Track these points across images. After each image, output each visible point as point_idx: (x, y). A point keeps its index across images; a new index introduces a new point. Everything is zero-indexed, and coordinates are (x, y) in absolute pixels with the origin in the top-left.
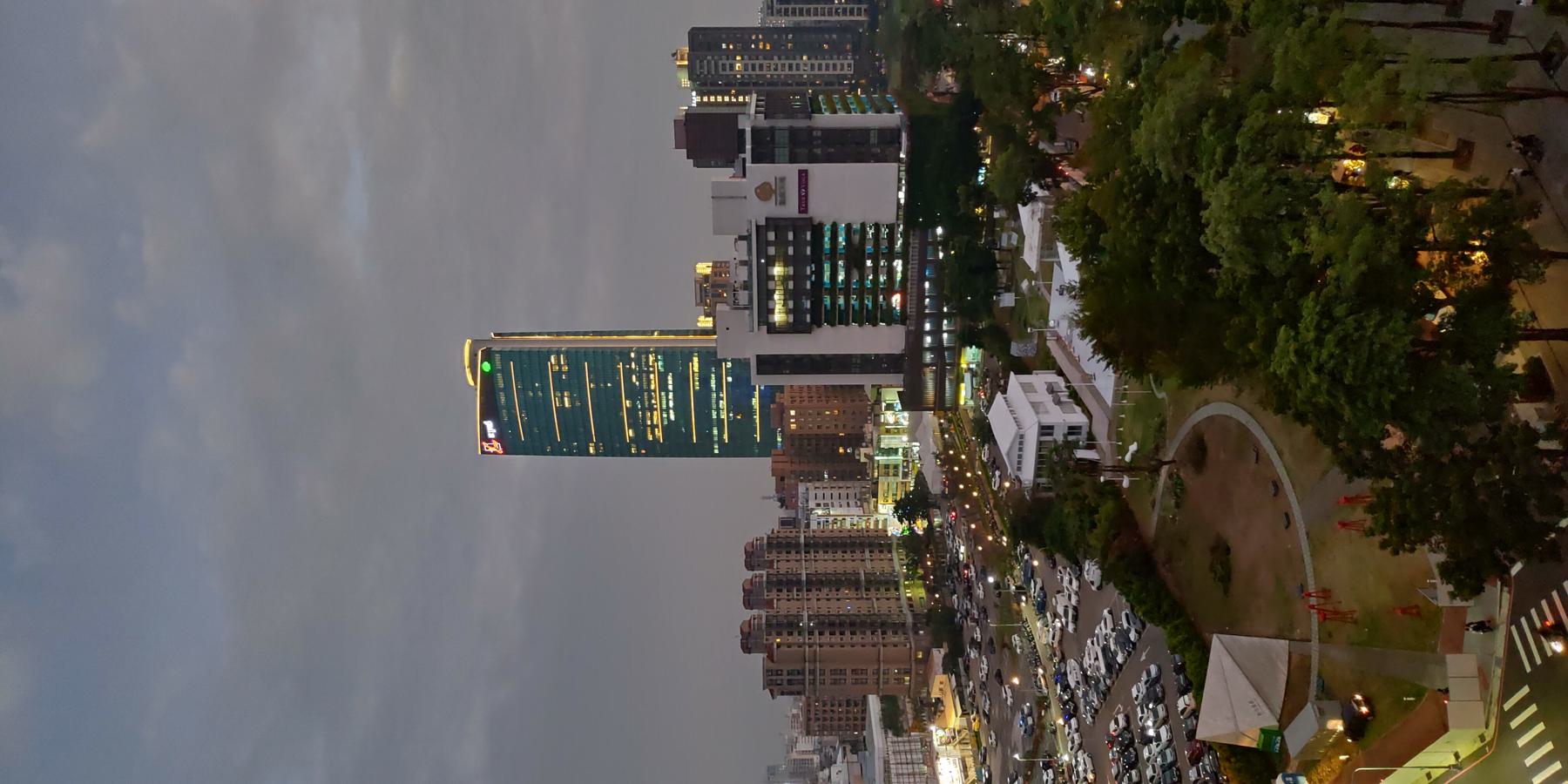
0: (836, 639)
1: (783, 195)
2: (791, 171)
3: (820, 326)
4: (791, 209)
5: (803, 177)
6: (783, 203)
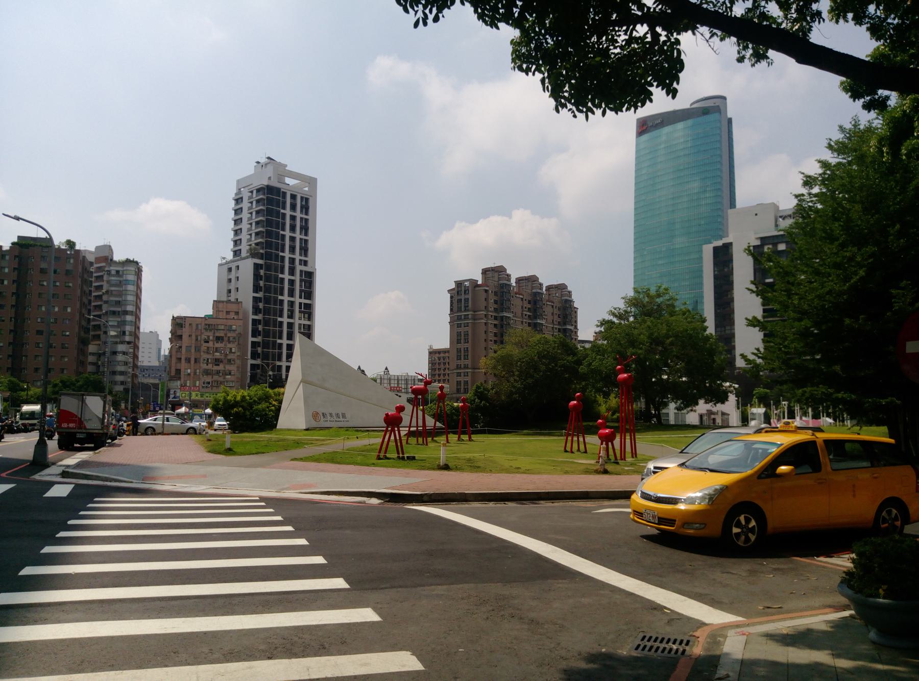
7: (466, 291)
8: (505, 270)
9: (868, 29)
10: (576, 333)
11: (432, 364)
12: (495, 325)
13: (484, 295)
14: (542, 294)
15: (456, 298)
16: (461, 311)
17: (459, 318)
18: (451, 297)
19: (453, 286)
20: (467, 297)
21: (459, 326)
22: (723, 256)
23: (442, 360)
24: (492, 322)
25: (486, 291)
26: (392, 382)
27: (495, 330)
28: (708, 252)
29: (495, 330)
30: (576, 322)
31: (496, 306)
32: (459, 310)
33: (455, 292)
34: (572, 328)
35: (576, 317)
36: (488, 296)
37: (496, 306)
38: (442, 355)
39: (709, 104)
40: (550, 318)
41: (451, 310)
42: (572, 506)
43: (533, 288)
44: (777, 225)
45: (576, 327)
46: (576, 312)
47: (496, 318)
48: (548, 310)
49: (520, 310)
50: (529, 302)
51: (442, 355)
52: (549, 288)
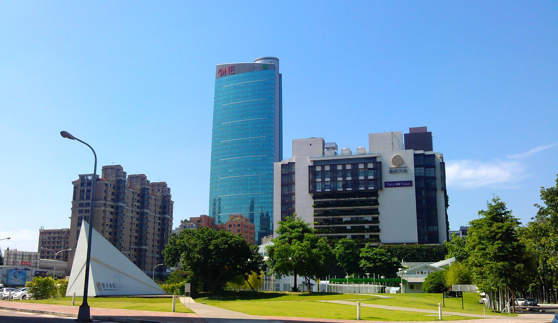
0: (108, 222)
1: (396, 172)
2: (411, 176)
3: (314, 198)
4: (387, 177)
5: (408, 184)
6: (391, 172)
7: (89, 183)
8: (122, 169)
9: (375, 163)
10: (171, 221)
11: (42, 242)
12: (111, 213)
13: (104, 188)
14: (125, 181)
15: (80, 188)
16: (83, 199)
17: (81, 205)
18: (75, 188)
19: (78, 178)
20: (89, 188)
21: (81, 211)
22: (288, 171)
23: (52, 240)
24: (109, 209)
25: (106, 185)
26: (18, 257)
27: (111, 217)
28: (277, 166)
29: (111, 217)
30: (172, 212)
31: (113, 197)
32: (82, 198)
33: (79, 183)
34: (169, 217)
35: (172, 209)
36: (107, 188)
37: (113, 197)
38: (52, 235)
39: (267, 62)
40: (130, 201)
41: (74, 198)
42: (297, 316)
43: (117, 176)
44: (324, 153)
45: (172, 216)
46: (172, 205)
47: (112, 207)
48: (152, 202)
49: (132, 201)
50: (139, 196)
51: (52, 235)
52: (131, 177)
